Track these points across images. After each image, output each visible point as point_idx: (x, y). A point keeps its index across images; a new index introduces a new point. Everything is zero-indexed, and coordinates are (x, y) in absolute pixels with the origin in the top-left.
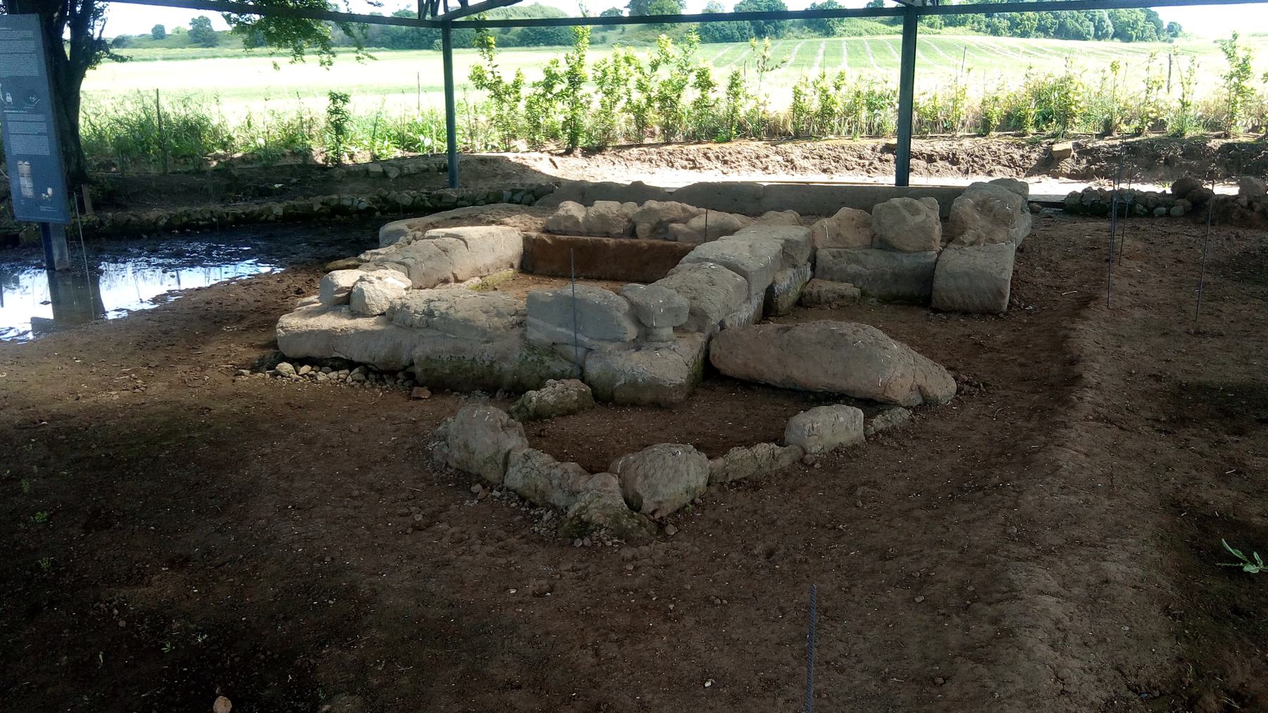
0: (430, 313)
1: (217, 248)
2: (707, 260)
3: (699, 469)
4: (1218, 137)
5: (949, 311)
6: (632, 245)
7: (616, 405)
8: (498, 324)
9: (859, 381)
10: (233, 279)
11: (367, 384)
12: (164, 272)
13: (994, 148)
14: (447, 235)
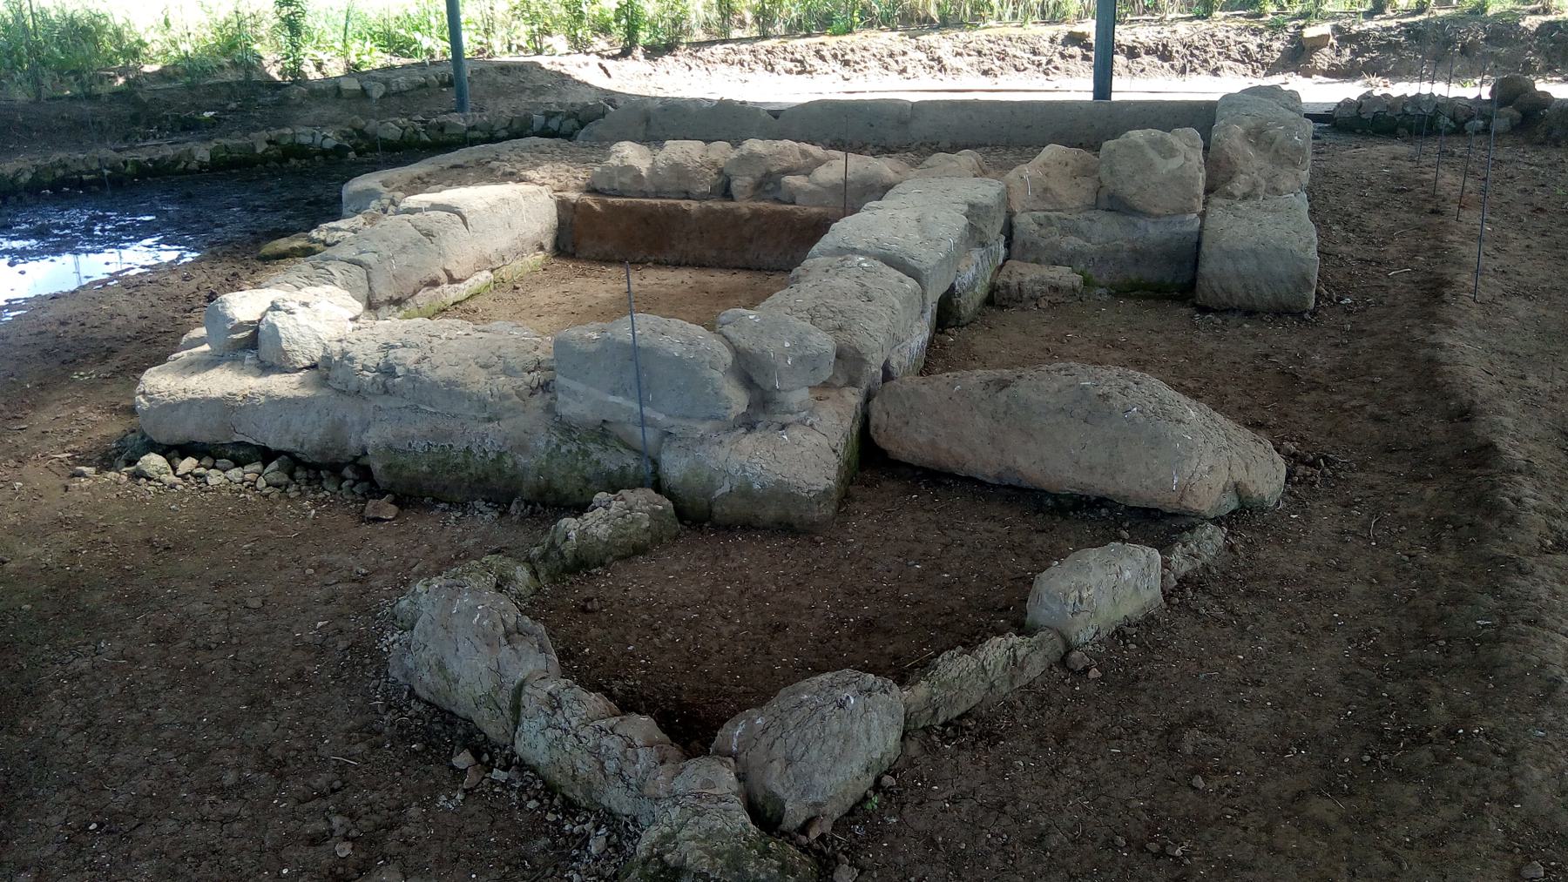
0: (388, 371)
1: (104, 219)
2: (854, 251)
3: (888, 720)
4: (1535, 12)
5: (1225, 310)
6: (726, 212)
7: (717, 527)
8: (507, 389)
9: (1136, 480)
10: (114, 276)
11: (292, 492)
12: (11, 264)
13: (1221, 35)
14: (435, 207)
